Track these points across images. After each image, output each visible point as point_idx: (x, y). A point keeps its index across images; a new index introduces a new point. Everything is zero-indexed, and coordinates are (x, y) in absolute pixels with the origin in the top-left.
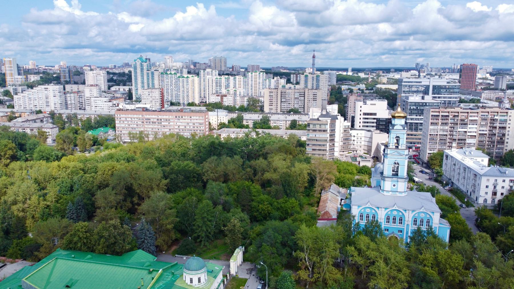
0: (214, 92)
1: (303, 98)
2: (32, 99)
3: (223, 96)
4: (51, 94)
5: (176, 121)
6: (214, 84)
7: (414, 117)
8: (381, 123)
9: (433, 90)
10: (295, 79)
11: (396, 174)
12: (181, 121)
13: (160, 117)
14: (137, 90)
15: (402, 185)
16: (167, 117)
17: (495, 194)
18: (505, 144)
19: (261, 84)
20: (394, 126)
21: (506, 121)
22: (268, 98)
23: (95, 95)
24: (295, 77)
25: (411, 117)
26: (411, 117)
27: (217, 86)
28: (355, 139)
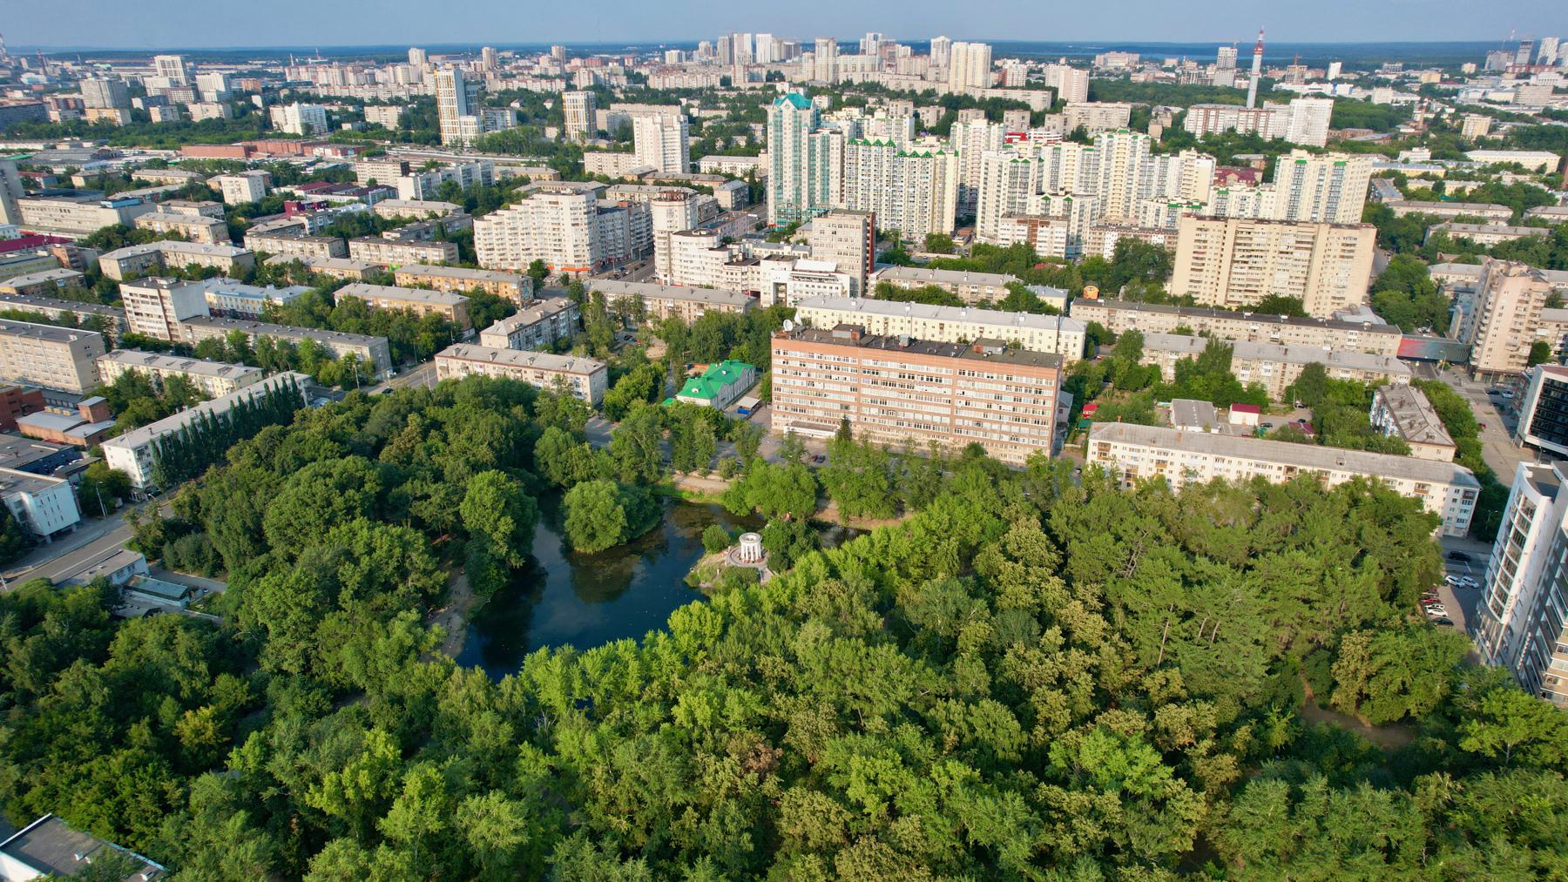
0: (1004, 208)
1: (1305, 255)
2: (520, 231)
3: (1034, 223)
4: (567, 219)
5: (961, 383)
6: (1006, 179)
10: (1200, 123)
12: (978, 385)
13: (910, 368)
14: (780, 187)
16: (933, 370)
19: (1136, 172)
22: (1192, 246)
23: (681, 227)
24: (1201, 118)
27: (1012, 185)
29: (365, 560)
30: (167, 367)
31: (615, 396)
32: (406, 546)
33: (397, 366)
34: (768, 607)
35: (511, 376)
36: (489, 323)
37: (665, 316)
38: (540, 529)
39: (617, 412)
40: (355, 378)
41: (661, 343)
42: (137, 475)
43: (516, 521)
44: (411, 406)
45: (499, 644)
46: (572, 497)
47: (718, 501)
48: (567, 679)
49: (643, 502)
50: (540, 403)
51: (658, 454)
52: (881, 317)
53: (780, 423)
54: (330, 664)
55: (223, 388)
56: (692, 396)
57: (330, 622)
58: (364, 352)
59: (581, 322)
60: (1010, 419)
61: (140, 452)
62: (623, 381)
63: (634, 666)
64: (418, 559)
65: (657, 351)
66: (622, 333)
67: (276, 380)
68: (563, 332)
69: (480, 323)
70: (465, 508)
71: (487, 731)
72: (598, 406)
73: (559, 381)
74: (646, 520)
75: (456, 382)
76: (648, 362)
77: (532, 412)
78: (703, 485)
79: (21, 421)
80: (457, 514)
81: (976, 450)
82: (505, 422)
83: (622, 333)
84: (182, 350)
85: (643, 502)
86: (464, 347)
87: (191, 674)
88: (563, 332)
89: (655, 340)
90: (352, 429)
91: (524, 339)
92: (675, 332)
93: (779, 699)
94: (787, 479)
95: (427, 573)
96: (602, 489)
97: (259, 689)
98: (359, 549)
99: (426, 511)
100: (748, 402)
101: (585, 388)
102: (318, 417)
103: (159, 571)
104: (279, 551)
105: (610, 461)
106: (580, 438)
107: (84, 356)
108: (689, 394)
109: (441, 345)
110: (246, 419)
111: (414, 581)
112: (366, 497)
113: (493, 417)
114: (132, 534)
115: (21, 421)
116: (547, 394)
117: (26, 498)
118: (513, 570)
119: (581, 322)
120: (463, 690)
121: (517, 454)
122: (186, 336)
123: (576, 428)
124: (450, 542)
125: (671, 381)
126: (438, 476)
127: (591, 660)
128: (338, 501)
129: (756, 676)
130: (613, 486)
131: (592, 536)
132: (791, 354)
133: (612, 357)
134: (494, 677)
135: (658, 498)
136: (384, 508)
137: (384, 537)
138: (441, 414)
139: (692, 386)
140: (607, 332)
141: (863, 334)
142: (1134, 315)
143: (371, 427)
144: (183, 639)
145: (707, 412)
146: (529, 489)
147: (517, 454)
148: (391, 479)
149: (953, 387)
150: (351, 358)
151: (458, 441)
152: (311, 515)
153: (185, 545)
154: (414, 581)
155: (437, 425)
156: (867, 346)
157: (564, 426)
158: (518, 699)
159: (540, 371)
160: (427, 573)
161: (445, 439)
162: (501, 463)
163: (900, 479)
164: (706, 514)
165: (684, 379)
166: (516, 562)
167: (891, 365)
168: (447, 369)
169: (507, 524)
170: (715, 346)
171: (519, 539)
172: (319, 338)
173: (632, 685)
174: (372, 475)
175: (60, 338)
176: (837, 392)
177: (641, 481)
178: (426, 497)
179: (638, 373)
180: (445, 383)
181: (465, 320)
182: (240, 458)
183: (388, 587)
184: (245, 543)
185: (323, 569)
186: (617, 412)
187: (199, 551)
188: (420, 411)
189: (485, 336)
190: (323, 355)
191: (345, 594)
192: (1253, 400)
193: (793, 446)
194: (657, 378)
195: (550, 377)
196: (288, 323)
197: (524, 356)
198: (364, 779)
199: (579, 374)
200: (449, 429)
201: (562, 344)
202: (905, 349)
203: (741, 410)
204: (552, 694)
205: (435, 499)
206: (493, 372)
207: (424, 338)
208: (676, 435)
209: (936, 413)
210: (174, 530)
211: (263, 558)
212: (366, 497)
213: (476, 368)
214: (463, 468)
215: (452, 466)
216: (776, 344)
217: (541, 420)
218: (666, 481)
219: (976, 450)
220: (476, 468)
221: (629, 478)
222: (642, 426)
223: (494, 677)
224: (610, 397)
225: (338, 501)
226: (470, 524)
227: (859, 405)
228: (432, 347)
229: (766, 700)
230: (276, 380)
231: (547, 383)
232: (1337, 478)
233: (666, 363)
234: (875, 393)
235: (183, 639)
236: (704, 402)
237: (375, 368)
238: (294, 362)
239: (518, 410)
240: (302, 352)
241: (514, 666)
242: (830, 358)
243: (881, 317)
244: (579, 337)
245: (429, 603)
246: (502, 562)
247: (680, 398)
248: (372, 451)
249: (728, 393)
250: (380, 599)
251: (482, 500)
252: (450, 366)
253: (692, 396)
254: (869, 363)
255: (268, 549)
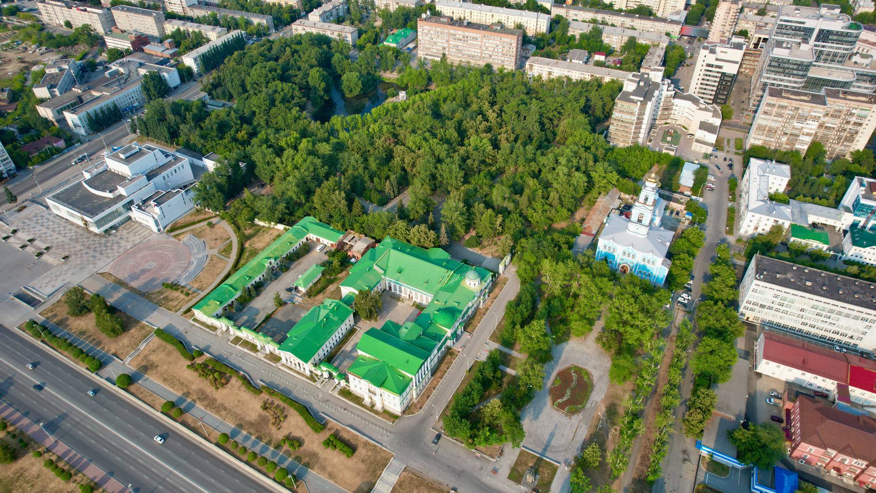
7: (773, 76)
8: (726, 79)
9: (818, 36)
11: (640, 221)
13: (467, 34)
15: (644, 231)
16: (474, 35)
17: (756, 228)
18: (855, 142)
20: (646, 186)
21: (860, 125)
25: (768, 75)
26: (768, 75)
28: (677, 108)
29: (282, 93)
30: (191, 28)
31: (359, 42)
32: (293, 89)
33: (276, 28)
34: (400, 108)
35: (322, 33)
36: (311, 11)
37: (383, 7)
38: (333, 89)
39: (361, 48)
40: (261, 33)
41: (381, 19)
42: (195, 68)
43: (327, 84)
44: (286, 44)
45: (323, 114)
46: (344, 77)
47: (395, 82)
48: (342, 122)
49: (368, 80)
50: (333, 44)
51: (375, 64)
52: (469, 11)
53: (421, 53)
54: (274, 122)
55: (215, 37)
56: (390, 43)
57: (274, 110)
58: (264, 22)
59: (348, 9)
60: (501, 53)
61: (195, 60)
62: (364, 36)
63: (360, 120)
64: (297, 93)
65: (379, 23)
66: (365, 14)
67: (235, 33)
68: (341, 14)
69: (307, 9)
70: (309, 79)
71: (321, 134)
72: (354, 46)
73: (339, 35)
74: (369, 87)
75: (301, 35)
76: (375, 28)
77: (330, 47)
78: (391, 76)
79: (144, 48)
80: (307, 82)
81: (489, 66)
82: (321, 51)
83: (365, 14)
84: (191, 19)
85: (368, 80)
86: (303, 20)
87: (236, 124)
88: (341, 14)
89: (378, 17)
90: (267, 53)
91: (325, 17)
92: (386, 15)
93: (397, 128)
94: (417, 73)
95: (300, 98)
96: (355, 74)
97: (255, 129)
98: (279, 89)
99: (297, 80)
100: (411, 46)
101: (349, 38)
102: (254, 48)
103: (213, 98)
104: (251, 92)
105: (357, 66)
106: (347, 57)
107: (158, 21)
108: (388, 42)
109: (293, 20)
110: (228, 49)
111: (296, 100)
112: (278, 75)
113: (317, 49)
114: (201, 87)
115: (144, 48)
116: (335, 40)
117: (165, 74)
118: (326, 101)
119: (348, 9)
120: (314, 125)
121: (325, 62)
122: (190, 13)
123: (346, 54)
124: (306, 89)
125: (383, 36)
126: (299, 69)
127: (349, 118)
128: (270, 76)
129: (393, 124)
130: (358, 74)
131: (351, 91)
132: (425, 27)
133: (360, 26)
134: (323, 123)
135: (375, 80)
136: (284, 78)
137: (287, 86)
138: (298, 47)
139: (390, 39)
140: (358, 15)
141: (452, 19)
142: (576, 12)
143: (274, 51)
144: (233, 114)
145: (393, 48)
146: (330, 74)
147: (325, 62)
148: (285, 69)
149: (482, 41)
150: (259, 24)
151: (305, 57)
152: (262, 80)
153: (219, 90)
154: (296, 100)
155: (296, 51)
156: (452, 25)
157: (341, 53)
158: (329, 128)
159: (333, 31)
160: (300, 98)
161: (300, 56)
162: (320, 65)
163: (452, 74)
164: (390, 85)
165: (387, 36)
166: (326, 98)
167: (460, 33)
168: (297, 30)
169: (323, 85)
170: (401, 22)
171: (327, 90)
172: (246, 16)
173: (360, 125)
174: (279, 68)
175: (150, 14)
176: (441, 42)
177: (368, 73)
178: (296, 76)
179: (370, 33)
180: (296, 36)
181: (301, 8)
182: (230, 62)
183: (289, 102)
184: (240, 89)
185: (269, 95)
186: (361, 48)
187: (224, 93)
188: (289, 46)
189: (310, 15)
190: (248, 23)
191: (277, 103)
192: (608, 52)
193: (423, 64)
194: (377, 35)
195: (336, 34)
196: (230, 8)
197: (326, 25)
198: (292, 140)
199: (346, 33)
200: (301, 53)
201: (341, 19)
202: (465, 27)
203: (408, 49)
204: (338, 126)
205: (300, 76)
206: (314, 31)
207: (286, 16)
208: (381, 57)
209: (476, 51)
210: (215, 86)
211: (247, 94)
212: (278, 75)
213: (308, 30)
214: (307, 67)
215: (304, 66)
216: (420, 24)
217: (333, 50)
218: (377, 74)
219: (489, 66)
220: (312, 67)
221: (364, 72)
222: (368, 53)
223: (323, 123)
224: (359, 42)
225: (270, 76)
226: (311, 83)
227: (449, 48)
228: (289, 20)
229: (394, 129)
230: (235, 33)
231: (335, 36)
232: (607, 79)
233: (381, 29)
234: (454, 43)
235: (233, 114)
236: (394, 45)
237: (269, 29)
238: (237, 26)
239: (325, 46)
240: (240, 22)
241: (328, 120)
242: (439, 29)
243: (469, 11)
244: (348, 16)
245: (302, 108)
246: (322, 98)
247: (385, 43)
248: (276, 60)
249: (404, 41)
250: (287, 104)
251: (315, 77)
252: (298, 28)
253: (390, 43)
254: (452, 31)
255: (247, 91)
